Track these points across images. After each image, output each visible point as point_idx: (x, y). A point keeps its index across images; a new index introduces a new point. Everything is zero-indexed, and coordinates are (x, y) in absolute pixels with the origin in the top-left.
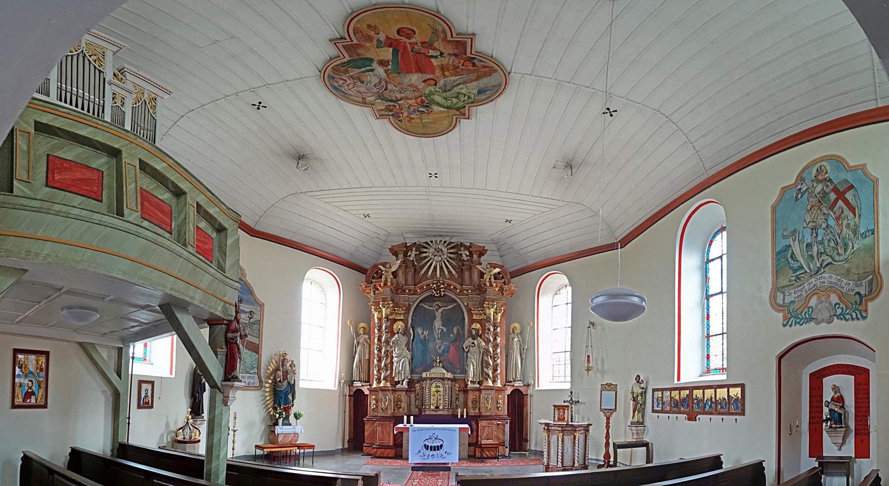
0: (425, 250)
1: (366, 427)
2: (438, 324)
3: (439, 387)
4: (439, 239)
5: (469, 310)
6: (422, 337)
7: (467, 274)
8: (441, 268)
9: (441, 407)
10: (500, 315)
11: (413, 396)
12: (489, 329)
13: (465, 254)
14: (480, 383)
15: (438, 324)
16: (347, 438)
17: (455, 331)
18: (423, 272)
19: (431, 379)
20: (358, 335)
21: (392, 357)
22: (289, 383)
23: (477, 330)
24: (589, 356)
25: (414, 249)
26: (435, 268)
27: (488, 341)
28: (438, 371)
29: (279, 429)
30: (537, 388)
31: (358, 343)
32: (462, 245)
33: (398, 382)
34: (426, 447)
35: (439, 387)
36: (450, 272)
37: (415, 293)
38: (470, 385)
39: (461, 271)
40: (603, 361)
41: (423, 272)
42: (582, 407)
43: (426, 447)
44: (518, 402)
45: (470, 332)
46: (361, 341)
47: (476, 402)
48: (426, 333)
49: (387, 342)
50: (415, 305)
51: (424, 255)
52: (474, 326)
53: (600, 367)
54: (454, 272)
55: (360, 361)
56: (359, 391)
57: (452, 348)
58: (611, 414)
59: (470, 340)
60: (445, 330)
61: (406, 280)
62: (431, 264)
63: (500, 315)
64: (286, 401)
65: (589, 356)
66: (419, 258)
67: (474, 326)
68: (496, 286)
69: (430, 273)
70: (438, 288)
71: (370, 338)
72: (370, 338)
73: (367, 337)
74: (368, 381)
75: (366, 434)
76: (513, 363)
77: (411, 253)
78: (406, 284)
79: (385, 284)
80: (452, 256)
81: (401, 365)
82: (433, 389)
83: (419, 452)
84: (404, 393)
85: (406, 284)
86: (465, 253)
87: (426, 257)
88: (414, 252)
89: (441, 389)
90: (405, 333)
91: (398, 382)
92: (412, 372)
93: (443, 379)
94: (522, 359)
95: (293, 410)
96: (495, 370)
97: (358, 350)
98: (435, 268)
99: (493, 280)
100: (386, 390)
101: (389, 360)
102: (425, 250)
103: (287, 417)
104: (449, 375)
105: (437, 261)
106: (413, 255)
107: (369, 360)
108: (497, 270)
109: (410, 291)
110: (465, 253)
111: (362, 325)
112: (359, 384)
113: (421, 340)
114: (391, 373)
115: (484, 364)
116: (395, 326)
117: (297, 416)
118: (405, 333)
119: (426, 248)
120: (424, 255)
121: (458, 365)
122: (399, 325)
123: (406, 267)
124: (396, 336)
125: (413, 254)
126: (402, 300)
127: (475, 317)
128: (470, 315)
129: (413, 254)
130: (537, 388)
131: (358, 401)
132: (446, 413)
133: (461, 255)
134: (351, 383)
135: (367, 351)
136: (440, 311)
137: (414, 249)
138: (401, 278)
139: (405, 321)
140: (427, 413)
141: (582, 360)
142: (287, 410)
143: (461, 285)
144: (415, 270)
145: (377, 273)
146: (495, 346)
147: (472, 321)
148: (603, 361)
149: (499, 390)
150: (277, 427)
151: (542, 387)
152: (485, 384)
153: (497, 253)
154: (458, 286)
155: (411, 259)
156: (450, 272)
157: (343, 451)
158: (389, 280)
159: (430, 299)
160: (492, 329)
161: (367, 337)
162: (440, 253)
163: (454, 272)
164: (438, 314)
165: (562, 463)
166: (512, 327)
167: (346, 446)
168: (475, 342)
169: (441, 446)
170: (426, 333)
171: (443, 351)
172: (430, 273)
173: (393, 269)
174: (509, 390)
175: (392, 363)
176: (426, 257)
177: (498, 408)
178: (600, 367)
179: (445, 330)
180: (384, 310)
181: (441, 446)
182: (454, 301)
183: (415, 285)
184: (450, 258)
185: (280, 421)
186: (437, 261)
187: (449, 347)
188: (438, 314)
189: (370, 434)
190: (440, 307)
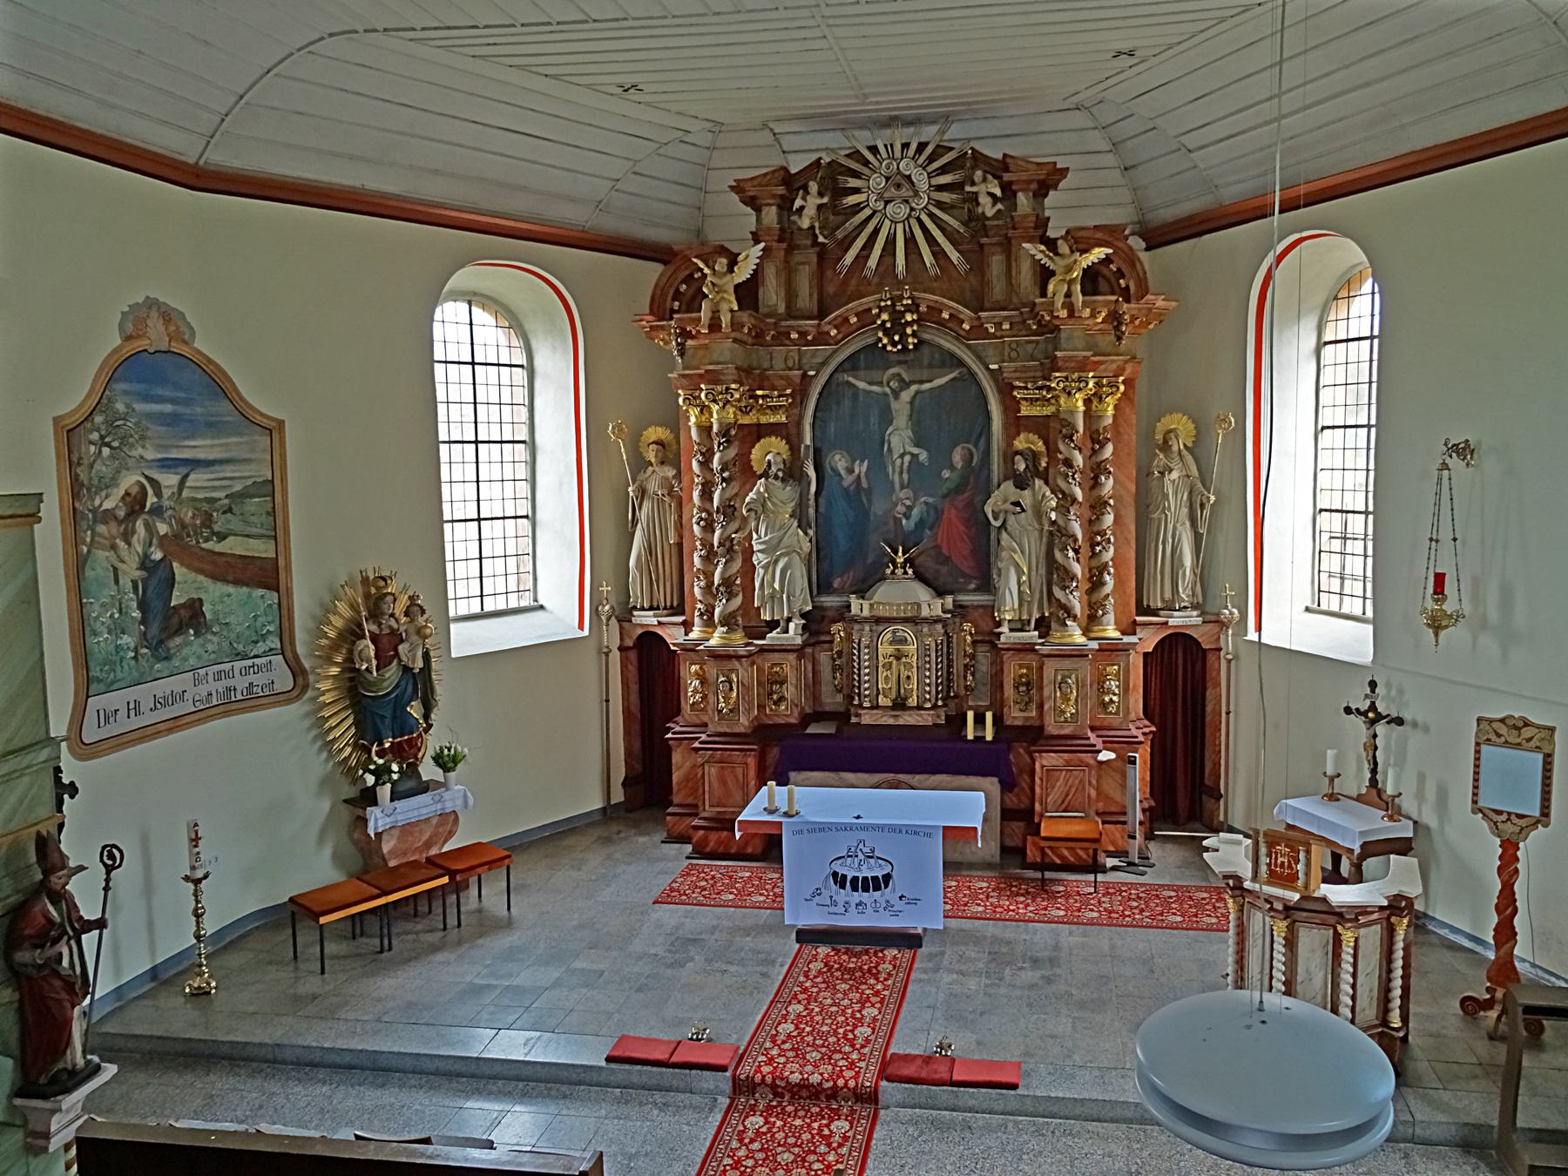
0: (853, 183)
1: (676, 758)
2: (900, 439)
3: (904, 641)
4: (899, 135)
5: (1005, 390)
6: (848, 480)
7: (996, 263)
8: (910, 241)
9: (913, 702)
10: (1110, 401)
11: (824, 657)
12: (1068, 463)
13: (995, 201)
14: (1043, 626)
15: (900, 439)
16: (619, 773)
17: (957, 457)
18: (849, 258)
19: (878, 620)
20: (640, 464)
21: (749, 552)
22: (406, 669)
23: (1033, 457)
24: (1440, 579)
25: (813, 187)
26: (891, 242)
27: (1066, 500)
28: (901, 593)
29: (377, 819)
30: (1252, 636)
31: (642, 492)
32: (978, 158)
33: (772, 625)
34: (840, 880)
35: (904, 641)
36: (939, 254)
37: (822, 338)
38: (1007, 636)
39: (977, 256)
40: (1507, 594)
41: (849, 258)
42: (1415, 740)
43: (840, 880)
44: (1183, 681)
45: (1010, 455)
46: (653, 486)
47: (1030, 685)
48: (861, 468)
49: (729, 510)
50: (822, 380)
51: (852, 200)
52: (1020, 443)
53: (1493, 615)
54: (954, 255)
55: (650, 549)
56: (650, 642)
57: (951, 514)
58: (1523, 832)
59: (1008, 486)
60: (923, 456)
61: (791, 296)
62: (876, 232)
63: (1110, 401)
64: (402, 724)
65: (1440, 579)
66: (835, 210)
67: (1020, 443)
68: (1093, 314)
69: (873, 262)
70: (898, 325)
71: (678, 476)
72: (678, 476)
73: (670, 473)
74: (678, 610)
75: (675, 778)
76: (1163, 551)
77: (807, 202)
78: (792, 313)
79: (715, 326)
80: (945, 197)
81: (781, 575)
82: (885, 649)
83: (817, 892)
84: (792, 657)
85: (792, 313)
86: (987, 189)
87: (857, 208)
88: (813, 201)
89: (912, 648)
90: (792, 473)
91: (772, 625)
92: (821, 585)
93: (914, 621)
94: (1197, 537)
95: (433, 743)
96: (1096, 583)
97: (643, 515)
98: (891, 242)
99: (1079, 298)
100: (729, 657)
101: (737, 564)
102: (853, 183)
103: (411, 770)
104: (932, 606)
105: (897, 214)
106: (810, 211)
107: (680, 545)
108: (1098, 253)
109: (803, 334)
110: (987, 189)
111: (655, 433)
112: (647, 619)
113: (846, 490)
114: (748, 597)
115: (1056, 573)
116: (756, 453)
117: (446, 762)
118: (792, 473)
119: (856, 175)
120: (852, 200)
121: (963, 562)
122: (769, 452)
123: (790, 250)
124: (760, 485)
125: (810, 204)
126: (779, 364)
127: (1025, 411)
128: (1010, 406)
129: (810, 204)
130: (1252, 636)
131: (652, 668)
132: (925, 719)
133: (974, 198)
134: (624, 615)
135: (671, 520)
136: (906, 396)
137: (813, 187)
138: (772, 295)
139: (789, 433)
140: (867, 718)
141: (1417, 581)
142: (407, 752)
143: (978, 307)
144: (821, 257)
145: (689, 279)
146: (1098, 506)
147: (1016, 423)
148: (1507, 594)
149: (1111, 650)
150: (373, 813)
151: (1274, 634)
152: (1056, 635)
153: (1110, 160)
154: (966, 313)
155: (805, 223)
156: (939, 254)
157: (608, 813)
158: (725, 319)
159: (871, 358)
160: (1079, 460)
161: (670, 473)
162: (905, 192)
163: (954, 255)
164: (900, 408)
165: (1338, 940)
166: (1160, 428)
167: (618, 796)
168: (1026, 497)
169: (887, 877)
170: (861, 468)
171: (921, 523)
172: (873, 262)
173: (743, 273)
174: (1147, 640)
175: (749, 569)
176: (857, 208)
177: (1104, 706)
178: (1493, 615)
179: (923, 456)
180: (715, 408)
181: (887, 877)
182: (961, 363)
183: (821, 315)
184: (940, 205)
185: (385, 791)
186: (897, 214)
187: (939, 513)
188: (900, 408)
189: (687, 779)
190: (905, 385)
